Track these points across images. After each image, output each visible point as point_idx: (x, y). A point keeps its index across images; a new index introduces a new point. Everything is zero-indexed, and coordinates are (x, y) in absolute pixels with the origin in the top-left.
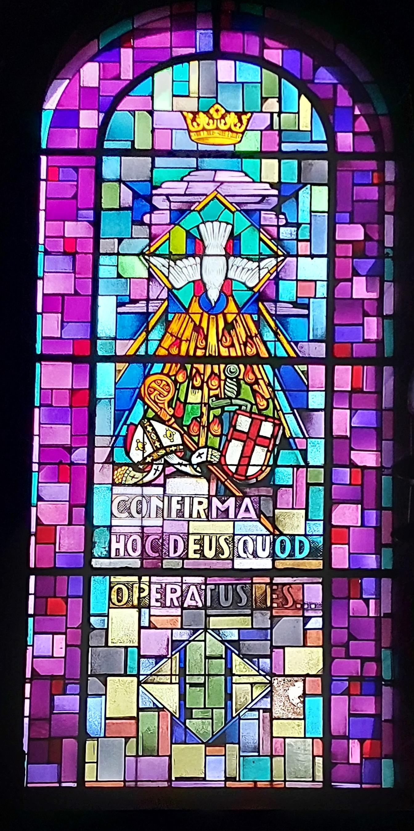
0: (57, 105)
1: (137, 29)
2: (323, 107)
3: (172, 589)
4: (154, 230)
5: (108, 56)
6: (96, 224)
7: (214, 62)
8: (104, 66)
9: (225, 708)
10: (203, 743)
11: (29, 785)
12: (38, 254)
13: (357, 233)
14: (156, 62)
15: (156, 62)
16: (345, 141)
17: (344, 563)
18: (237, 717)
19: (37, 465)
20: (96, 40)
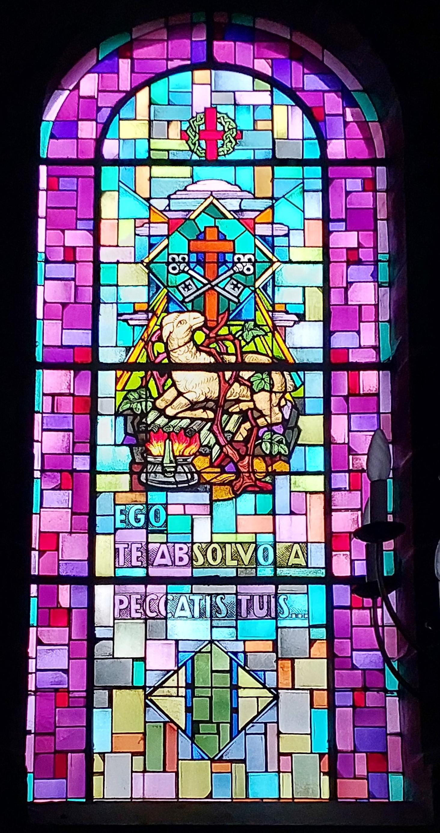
0: (57, 117)
1: (136, 39)
2: (314, 116)
3: (180, 561)
4: (153, 240)
5: (106, 67)
6: (96, 232)
8: (102, 77)
9: (231, 723)
13: (351, 239)
14: (153, 73)
15: (153, 73)
16: (337, 149)
19: (39, 473)
20: (95, 49)
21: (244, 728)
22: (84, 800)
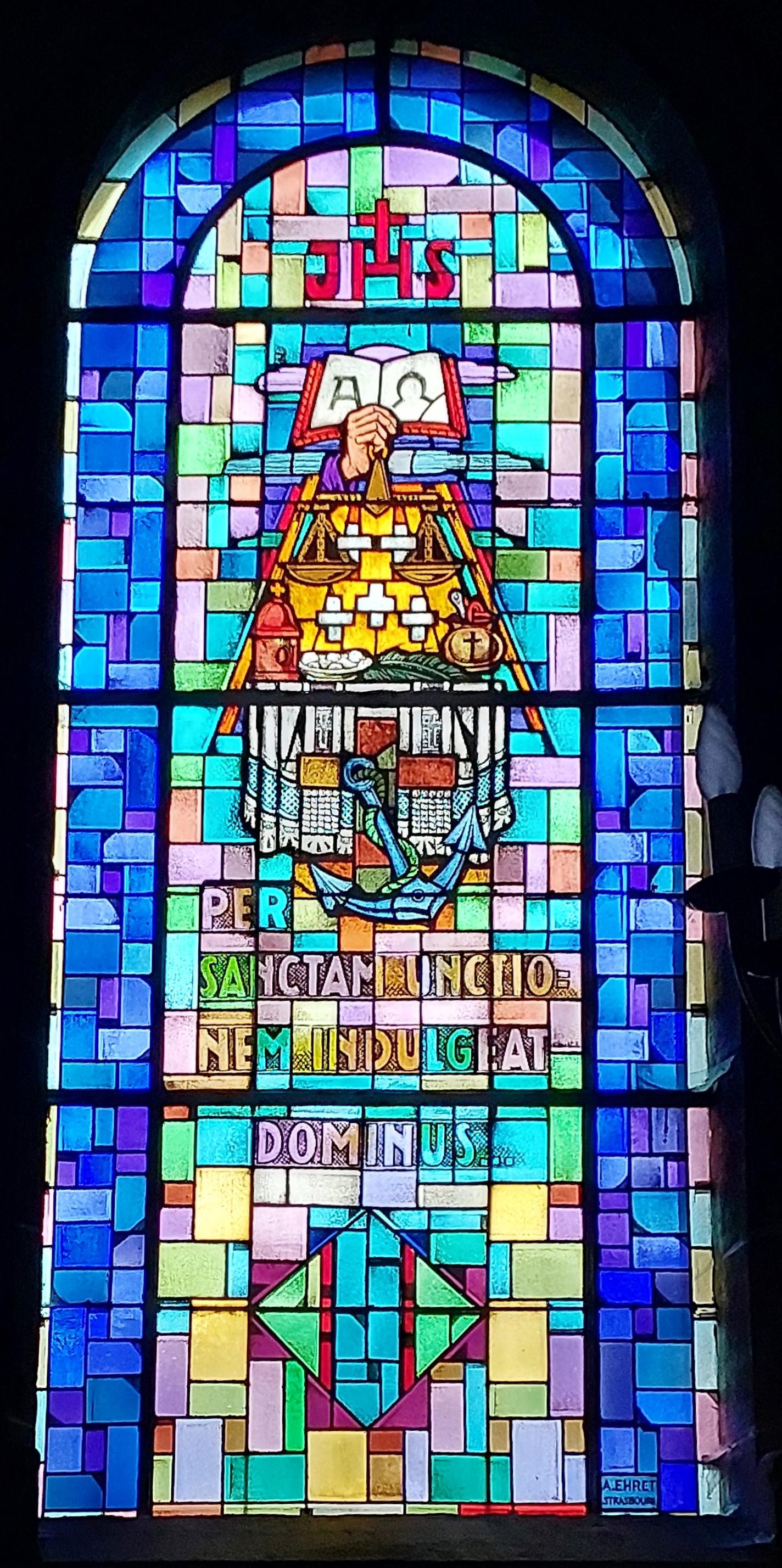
7: (245, 305)
10: (363, 1428)
11: (46, 1515)
12: (188, 279)
17: (155, 587)
18: (426, 1378)
21: (427, 1372)
22: (133, 1514)
